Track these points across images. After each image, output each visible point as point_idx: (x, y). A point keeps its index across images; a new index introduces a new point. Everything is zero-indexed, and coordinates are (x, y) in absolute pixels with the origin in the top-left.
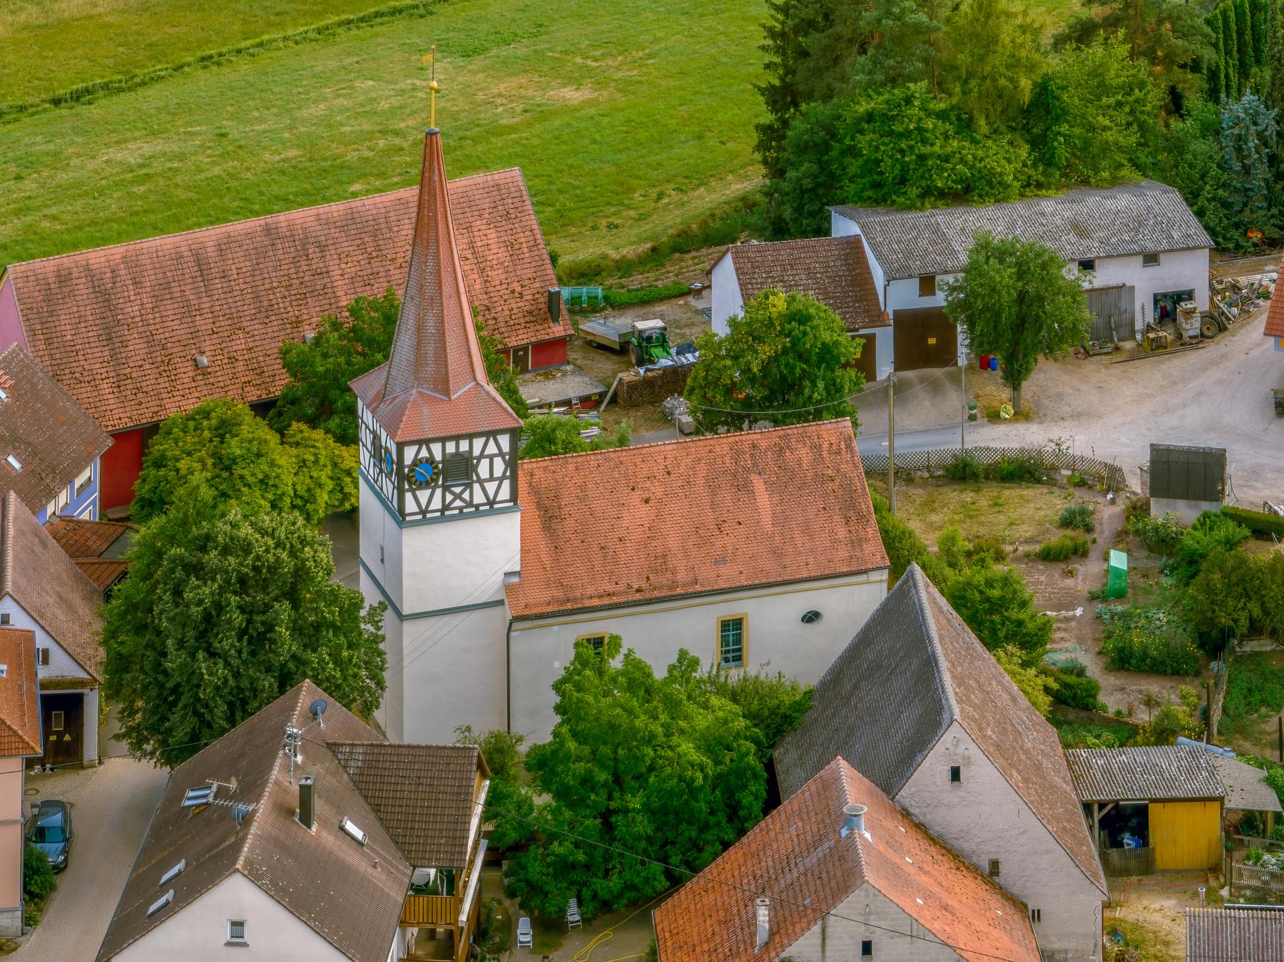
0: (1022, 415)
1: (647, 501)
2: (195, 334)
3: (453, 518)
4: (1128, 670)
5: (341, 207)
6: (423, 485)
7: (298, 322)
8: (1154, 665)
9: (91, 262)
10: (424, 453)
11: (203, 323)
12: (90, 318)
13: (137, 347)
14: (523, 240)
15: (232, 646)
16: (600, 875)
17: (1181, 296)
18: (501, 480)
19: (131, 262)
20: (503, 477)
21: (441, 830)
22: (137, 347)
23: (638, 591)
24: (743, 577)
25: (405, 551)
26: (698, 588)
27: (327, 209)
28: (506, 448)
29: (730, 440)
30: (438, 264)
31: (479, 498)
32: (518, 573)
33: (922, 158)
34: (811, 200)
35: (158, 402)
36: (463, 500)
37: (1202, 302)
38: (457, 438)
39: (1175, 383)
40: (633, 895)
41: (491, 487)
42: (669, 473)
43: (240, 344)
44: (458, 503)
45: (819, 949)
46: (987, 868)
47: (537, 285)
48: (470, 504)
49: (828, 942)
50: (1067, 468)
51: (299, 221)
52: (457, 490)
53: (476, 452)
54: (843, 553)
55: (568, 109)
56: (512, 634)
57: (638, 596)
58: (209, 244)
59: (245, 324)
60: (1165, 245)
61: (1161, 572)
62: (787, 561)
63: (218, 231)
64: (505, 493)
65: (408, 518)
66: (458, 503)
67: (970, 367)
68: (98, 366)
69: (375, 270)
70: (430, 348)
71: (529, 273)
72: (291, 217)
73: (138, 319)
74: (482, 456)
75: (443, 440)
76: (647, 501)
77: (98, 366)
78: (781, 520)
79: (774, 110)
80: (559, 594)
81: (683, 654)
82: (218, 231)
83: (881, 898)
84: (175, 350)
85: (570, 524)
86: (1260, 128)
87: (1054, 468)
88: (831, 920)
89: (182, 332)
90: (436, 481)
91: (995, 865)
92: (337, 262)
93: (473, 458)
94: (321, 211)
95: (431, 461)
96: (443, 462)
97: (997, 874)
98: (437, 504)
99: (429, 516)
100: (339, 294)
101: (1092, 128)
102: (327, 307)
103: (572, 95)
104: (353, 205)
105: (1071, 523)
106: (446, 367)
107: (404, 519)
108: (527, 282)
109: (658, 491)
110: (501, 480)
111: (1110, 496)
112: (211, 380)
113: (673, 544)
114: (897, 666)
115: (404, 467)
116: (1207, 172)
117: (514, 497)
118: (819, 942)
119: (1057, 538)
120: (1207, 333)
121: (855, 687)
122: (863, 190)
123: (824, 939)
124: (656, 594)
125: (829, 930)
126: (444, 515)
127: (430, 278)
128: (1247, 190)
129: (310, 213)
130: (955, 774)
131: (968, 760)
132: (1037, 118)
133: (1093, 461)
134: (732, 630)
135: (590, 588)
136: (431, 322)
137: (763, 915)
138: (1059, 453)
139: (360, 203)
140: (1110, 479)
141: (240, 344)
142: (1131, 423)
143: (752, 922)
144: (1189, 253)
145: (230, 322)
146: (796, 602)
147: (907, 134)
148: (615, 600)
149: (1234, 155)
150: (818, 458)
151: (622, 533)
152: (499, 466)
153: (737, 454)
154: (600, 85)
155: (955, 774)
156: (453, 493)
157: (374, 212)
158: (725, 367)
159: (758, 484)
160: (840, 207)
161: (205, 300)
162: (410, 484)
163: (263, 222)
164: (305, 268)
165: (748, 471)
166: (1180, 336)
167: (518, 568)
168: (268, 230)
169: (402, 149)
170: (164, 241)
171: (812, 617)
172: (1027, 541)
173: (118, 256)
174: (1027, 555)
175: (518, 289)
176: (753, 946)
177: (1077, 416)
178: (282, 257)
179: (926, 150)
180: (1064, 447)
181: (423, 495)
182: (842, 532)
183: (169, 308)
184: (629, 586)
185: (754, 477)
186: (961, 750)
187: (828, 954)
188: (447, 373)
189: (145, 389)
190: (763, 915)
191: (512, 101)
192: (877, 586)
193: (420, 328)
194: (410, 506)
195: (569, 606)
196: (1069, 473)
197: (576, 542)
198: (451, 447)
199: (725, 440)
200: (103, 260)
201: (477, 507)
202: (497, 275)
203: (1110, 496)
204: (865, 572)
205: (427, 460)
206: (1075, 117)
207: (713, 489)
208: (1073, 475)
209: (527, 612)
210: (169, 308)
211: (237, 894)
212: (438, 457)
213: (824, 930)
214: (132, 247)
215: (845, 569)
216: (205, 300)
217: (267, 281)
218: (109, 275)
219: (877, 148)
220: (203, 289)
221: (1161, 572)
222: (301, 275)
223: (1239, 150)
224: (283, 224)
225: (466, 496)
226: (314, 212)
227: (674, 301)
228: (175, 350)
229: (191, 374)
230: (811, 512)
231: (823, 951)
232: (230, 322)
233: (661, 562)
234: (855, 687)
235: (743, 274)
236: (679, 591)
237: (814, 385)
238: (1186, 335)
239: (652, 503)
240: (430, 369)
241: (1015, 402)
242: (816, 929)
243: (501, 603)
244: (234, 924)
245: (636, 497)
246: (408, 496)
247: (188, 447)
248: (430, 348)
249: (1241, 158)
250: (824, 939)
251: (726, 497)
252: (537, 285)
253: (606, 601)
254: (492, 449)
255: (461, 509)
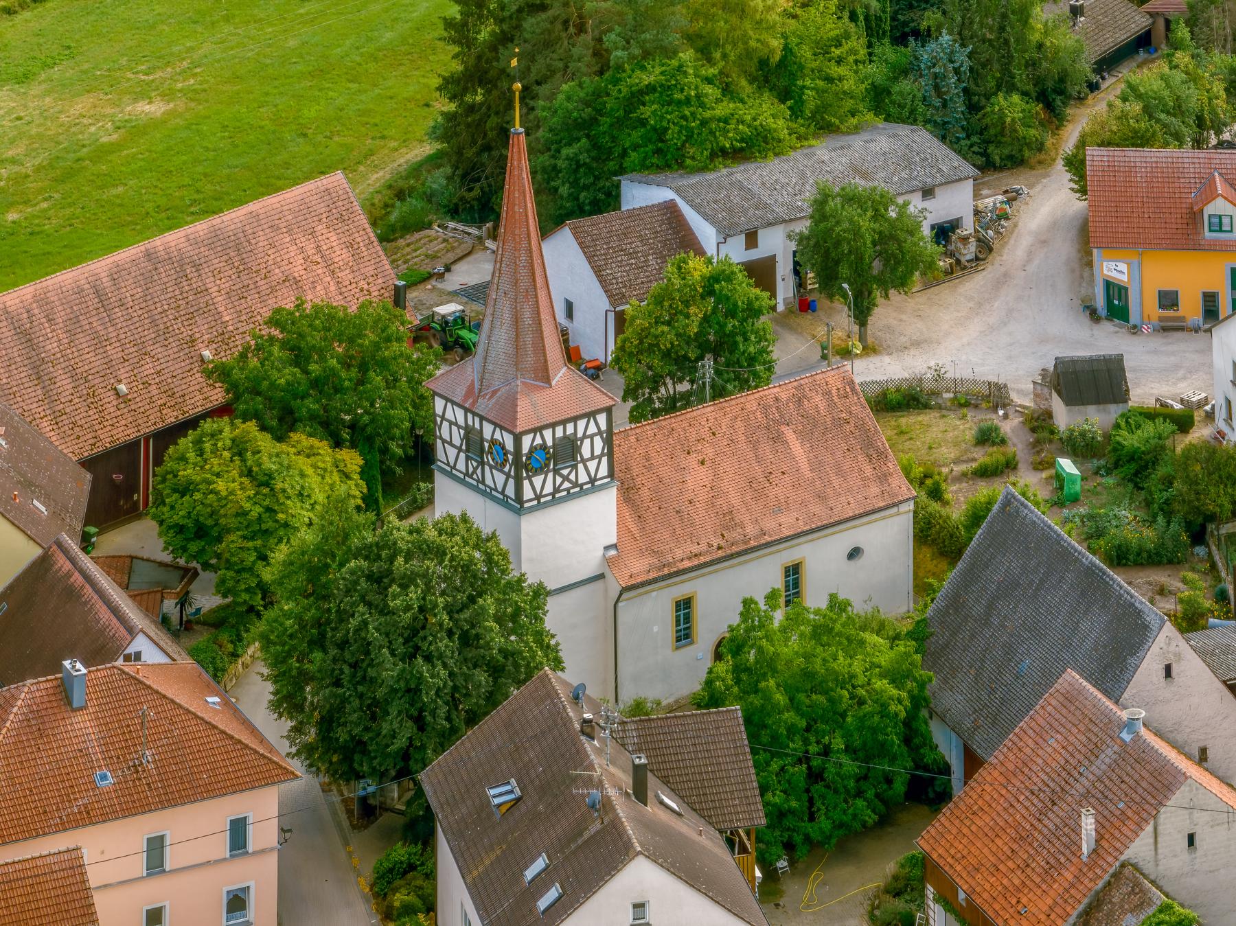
0: (870, 350)
1: (703, 463)
2: (109, 364)
3: (563, 500)
4: (1125, 565)
5: (205, 226)
6: (537, 471)
7: (192, 342)
8: (1149, 557)
9: (8, 304)
10: (538, 441)
11: (114, 352)
12: (18, 359)
13: (64, 383)
14: (359, 240)
15: (447, 646)
16: (806, 818)
17: (954, 225)
18: (600, 457)
19: (41, 300)
20: (602, 455)
21: (732, 792)
22: (64, 383)
23: (719, 548)
24: (801, 523)
25: (524, 537)
26: (767, 539)
27: (193, 230)
28: (603, 427)
29: (757, 396)
30: (531, 258)
31: (583, 478)
32: (615, 546)
33: (704, 123)
34: (585, 174)
35: (93, 434)
36: (570, 481)
37: (968, 227)
38: (563, 423)
39: (980, 305)
40: (841, 832)
41: (592, 465)
42: (714, 434)
43: (148, 369)
44: (567, 485)
45: (1152, 847)
46: (1196, 753)
47: (380, 281)
48: (575, 484)
49: (1159, 839)
50: (948, 391)
51: (173, 244)
52: (565, 472)
53: (580, 435)
54: (874, 490)
55: (154, 124)
56: (620, 604)
57: (720, 554)
58: (103, 275)
59: (149, 349)
60: (939, 179)
61: (1096, 473)
62: (831, 503)
63: (108, 261)
64: (603, 471)
65: (526, 505)
66: (567, 485)
67: (790, 311)
68: (35, 405)
69: (245, 283)
70: (528, 339)
71: (370, 270)
72: (165, 240)
73: (59, 355)
74: (585, 436)
75: (553, 426)
76: (703, 463)
77: (35, 405)
78: (817, 465)
79: (452, 98)
80: (654, 561)
81: (833, 598)
82: (108, 261)
83: (1202, 790)
84: (96, 381)
85: (645, 492)
86: (957, 65)
87: (934, 394)
88: (1162, 817)
89: (98, 363)
90: (547, 465)
91: (1203, 751)
92: (212, 279)
93: (577, 439)
94: (189, 231)
95: (544, 447)
96: (554, 446)
97: (1206, 760)
98: (549, 489)
99: (543, 500)
100: (220, 309)
101: (829, 79)
102: (213, 323)
103: (144, 107)
104: (214, 222)
105: (987, 440)
106: (545, 356)
107: (522, 506)
108: (371, 279)
109: (710, 452)
110: (600, 457)
111: (1001, 412)
112: (133, 407)
113: (735, 500)
114: (1041, 581)
115: (522, 456)
116: (916, 110)
117: (611, 474)
118: (1152, 840)
119: (982, 457)
120: (981, 256)
121: (990, 607)
122: (645, 159)
123: (1156, 838)
124: (735, 549)
125: (1160, 828)
126: (555, 500)
127: (523, 272)
128: (945, 123)
129: (178, 235)
130: (1168, 671)
131: (1178, 656)
132: (777, 76)
133: (974, 382)
134: (793, 572)
135: (679, 553)
136: (527, 314)
137: (1088, 824)
138: (938, 378)
139: (219, 221)
140: (996, 397)
141: (148, 369)
142: (969, 344)
143: (1077, 830)
144: (958, 184)
145: (136, 348)
146: (842, 541)
147: (688, 101)
148: (703, 559)
149: (933, 93)
150: (831, 405)
151: (690, 496)
152: (599, 443)
153: (765, 409)
154: (168, 96)
155: (1168, 671)
156: (561, 476)
157: (233, 227)
158: (663, 332)
159: (789, 434)
160: (629, 176)
161: (111, 329)
162: (527, 471)
163: (143, 248)
164: (187, 288)
165: (777, 423)
166: (958, 262)
167: (614, 540)
168: (148, 255)
169: (27, 176)
170: (64, 277)
171: (854, 553)
172: (957, 461)
173: (29, 296)
174: (964, 475)
175: (366, 287)
176: (1077, 853)
177: (917, 344)
178: (166, 280)
179: (708, 114)
180: (943, 371)
181: (538, 481)
182: (868, 471)
183: (83, 340)
184: (710, 545)
185: (784, 428)
186: (1172, 648)
187: (1160, 851)
188: (546, 361)
189: (79, 423)
190: (1088, 824)
191: (98, 121)
192: (905, 517)
193: (516, 321)
194: (528, 493)
195: (666, 571)
196: (952, 395)
197: (655, 509)
198: (559, 432)
199: (751, 397)
200: (17, 301)
201: (581, 486)
202: (345, 276)
203: (1001, 412)
204: (896, 505)
205: (541, 446)
206: (813, 71)
207: (755, 445)
208: (956, 397)
209: (633, 582)
210: (83, 340)
211: (641, 877)
212: (550, 443)
213: (1155, 829)
214: (39, 286)
215: (882, 504)
216: (111, 329)
217: (158, 305)
218: (25, 315)
219: (662, 117)
220: (107, 319)
221: (1096, 473)
222: (185, 295)
223: (937, 87)
224: (161, 248)
225: (572, 477)
226: (183, 234)
227: (421, 286)
228: (96, 381)
229: (115, 403)
230: (839, 455)
231: (1156, 849)
232: (136, 348)
233: (728, 520)
234: (990, 607)
235: (588, 247)
236: (753, 543)
237: (746, 339)
238: (963, 260)
239: (708, 463)
240: (530, 360)
241: (862, 338)
242: (1149, 828)
243: (601, 577)
244: (636, 906)
245: (693, 460)
246: (526, 483)
247: (216, 469)
248: (528, 339)
249: (939, 94)
250: (1156, 838)
251: (766, 449)
252: (380, 281)
253: (696, 562)
254: (592, 429)
255: (568, 490)
